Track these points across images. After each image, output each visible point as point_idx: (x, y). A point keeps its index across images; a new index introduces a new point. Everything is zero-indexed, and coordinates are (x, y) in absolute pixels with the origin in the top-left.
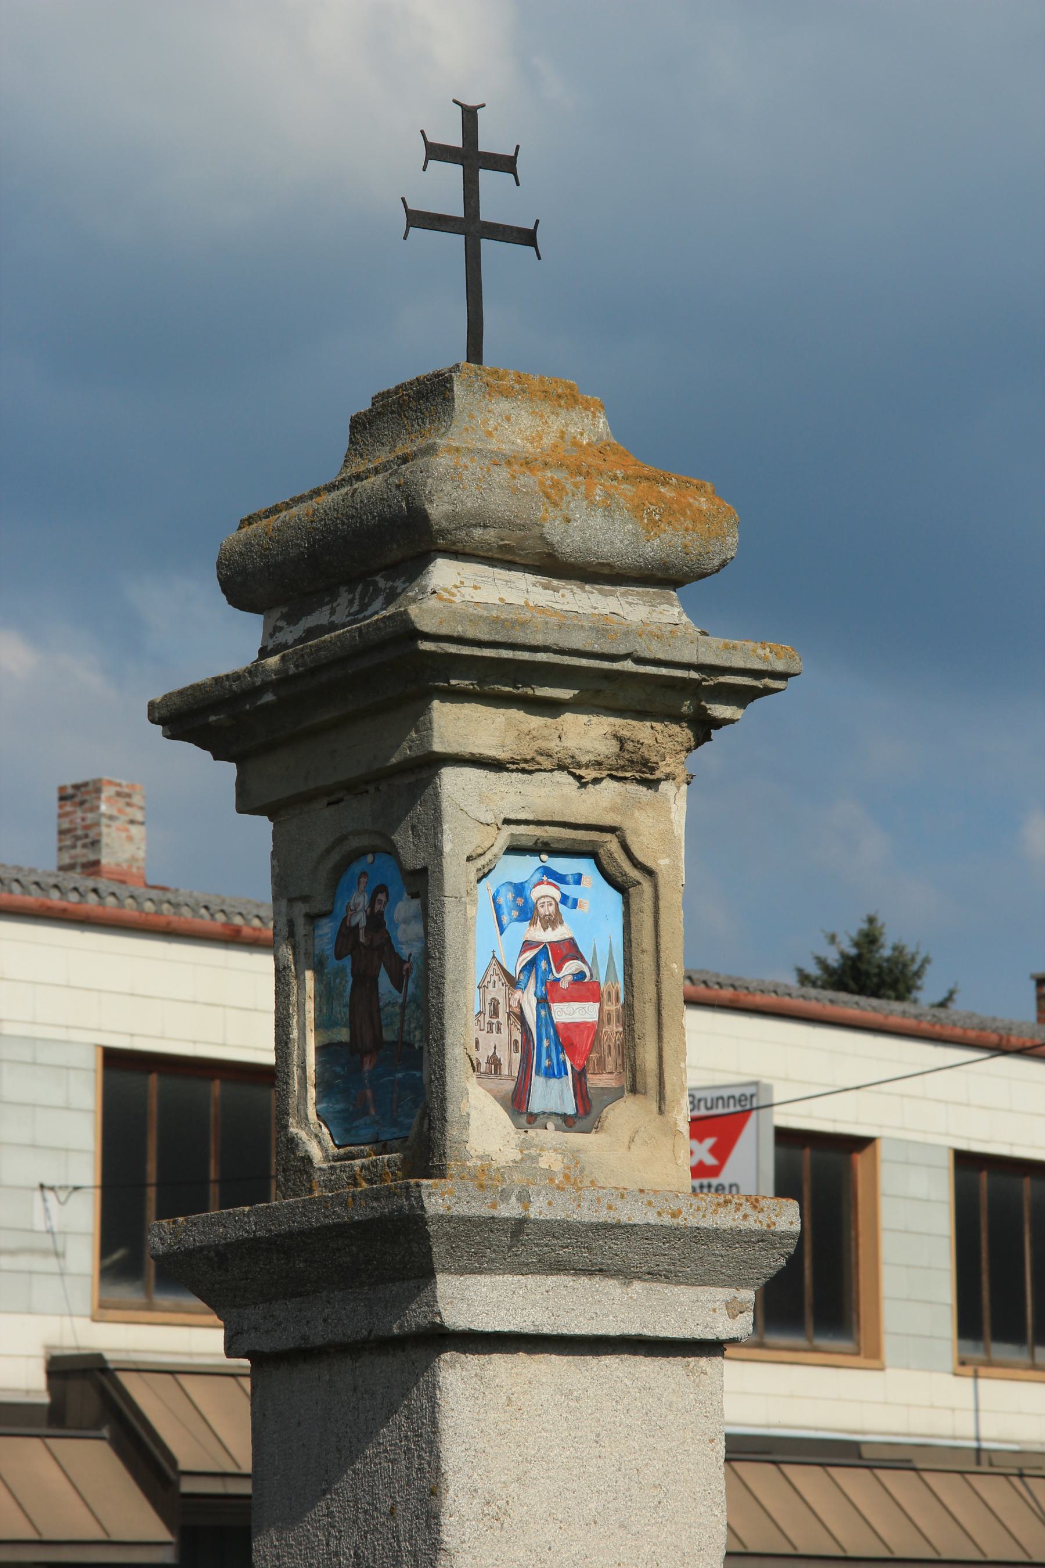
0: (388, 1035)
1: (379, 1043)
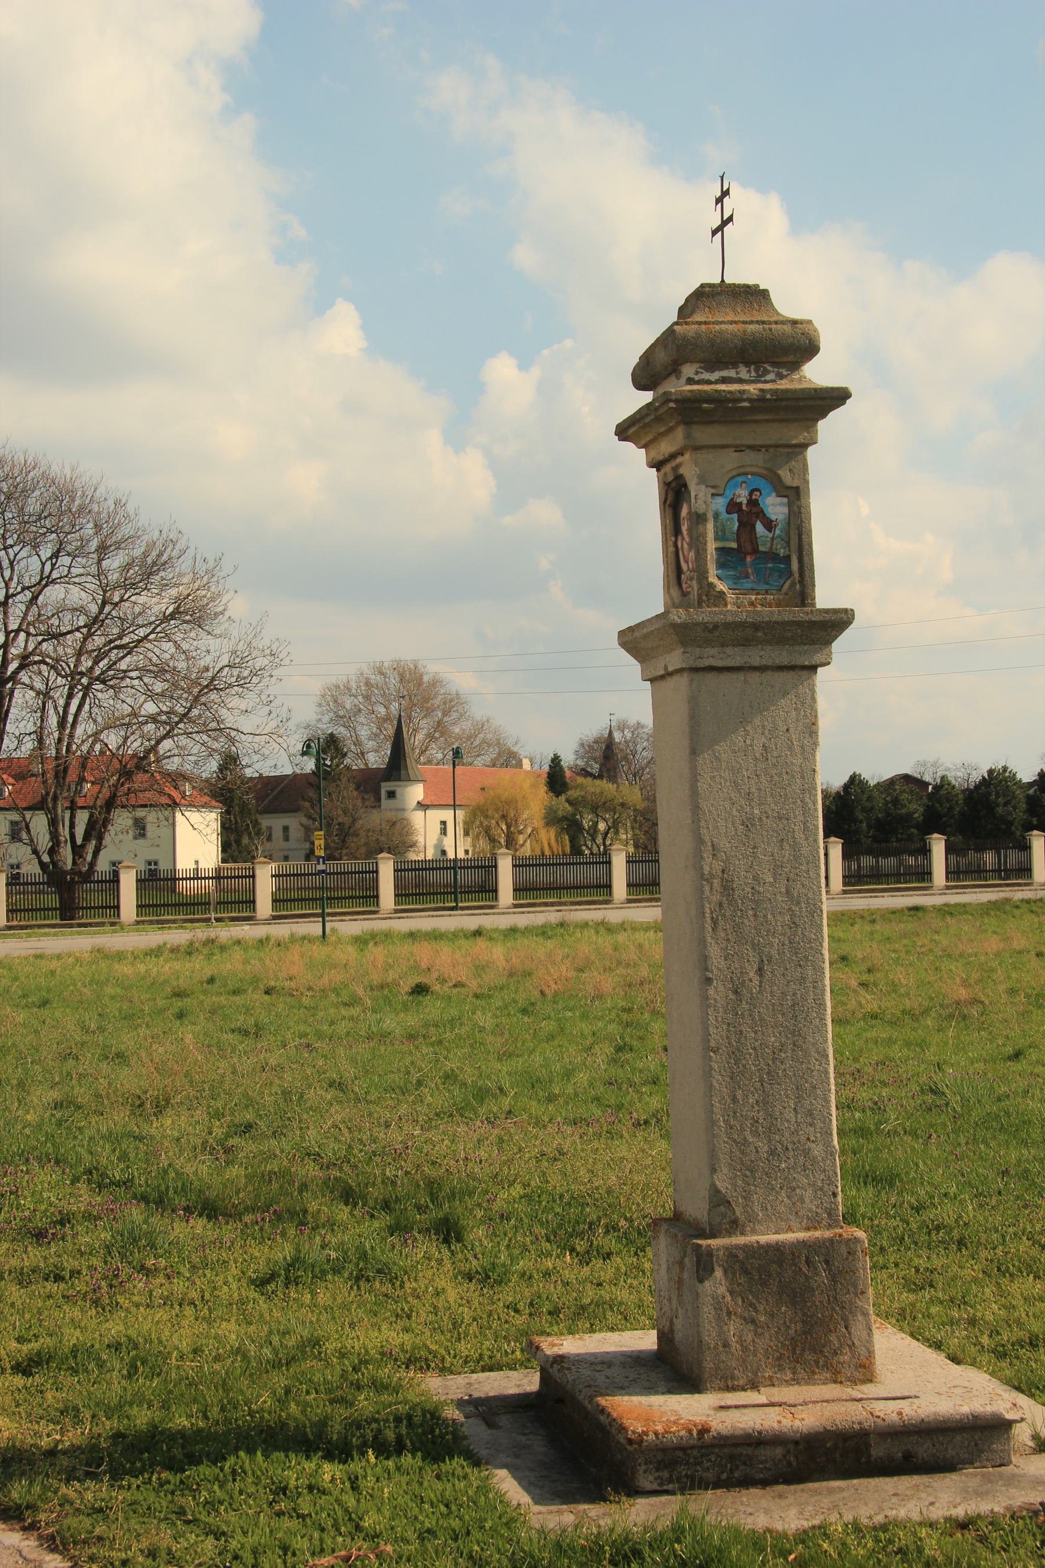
0: (761, 548)
1: (755, 551)
